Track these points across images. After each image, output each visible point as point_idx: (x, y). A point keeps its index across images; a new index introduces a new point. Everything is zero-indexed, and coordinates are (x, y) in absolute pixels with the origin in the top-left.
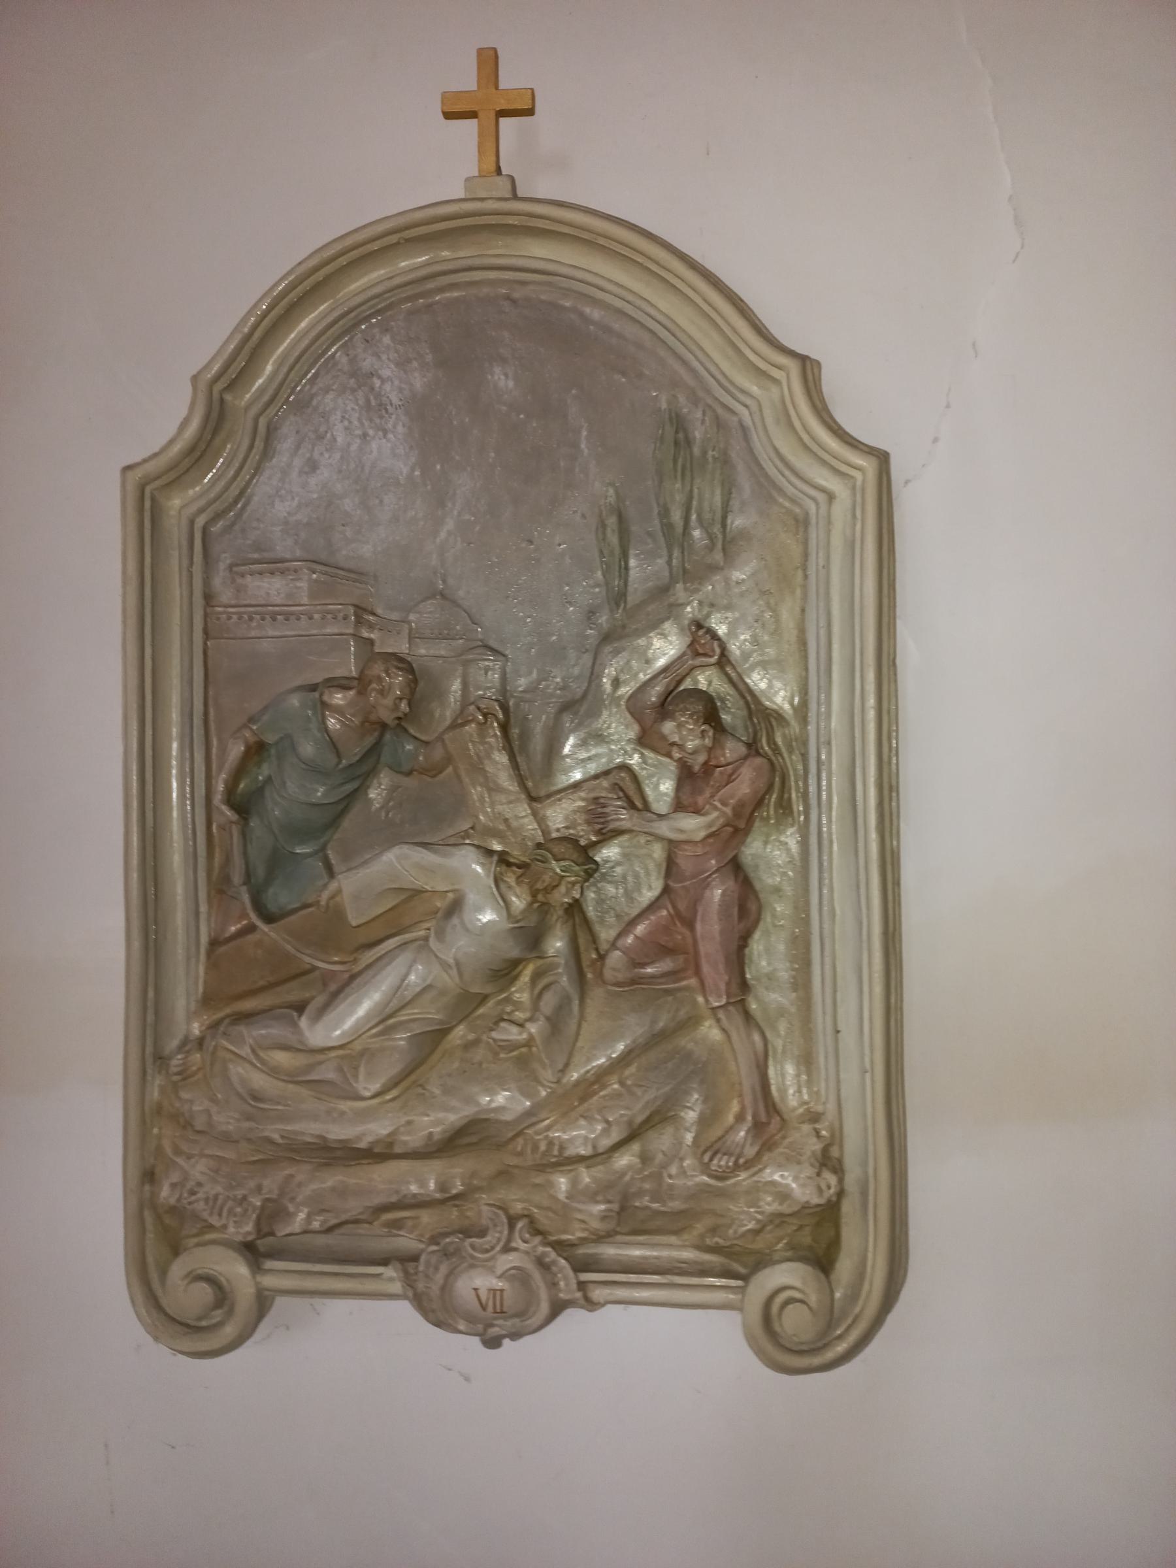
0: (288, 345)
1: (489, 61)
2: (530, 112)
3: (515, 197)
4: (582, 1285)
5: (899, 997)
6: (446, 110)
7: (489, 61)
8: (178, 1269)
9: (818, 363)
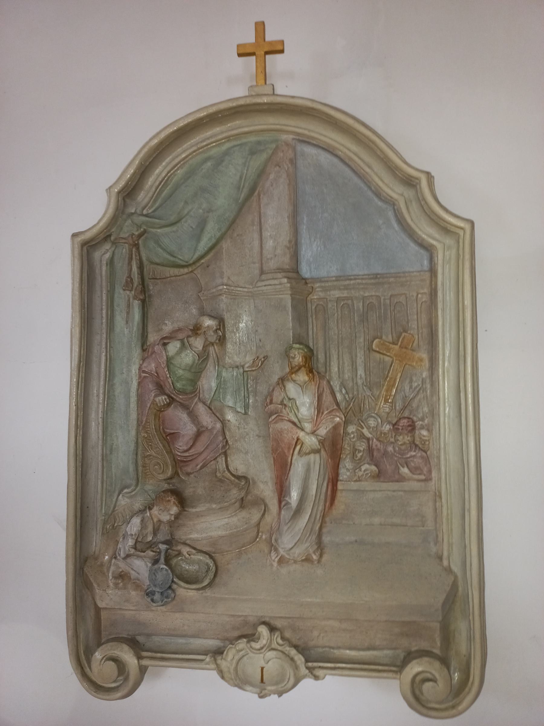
1: (260, 27)
2: (282, 51)
3: (274, 94)
5: (480, 541)
6: (238, 52)
7: (260, 27)
8: (98, 655)
9: (433, 177)
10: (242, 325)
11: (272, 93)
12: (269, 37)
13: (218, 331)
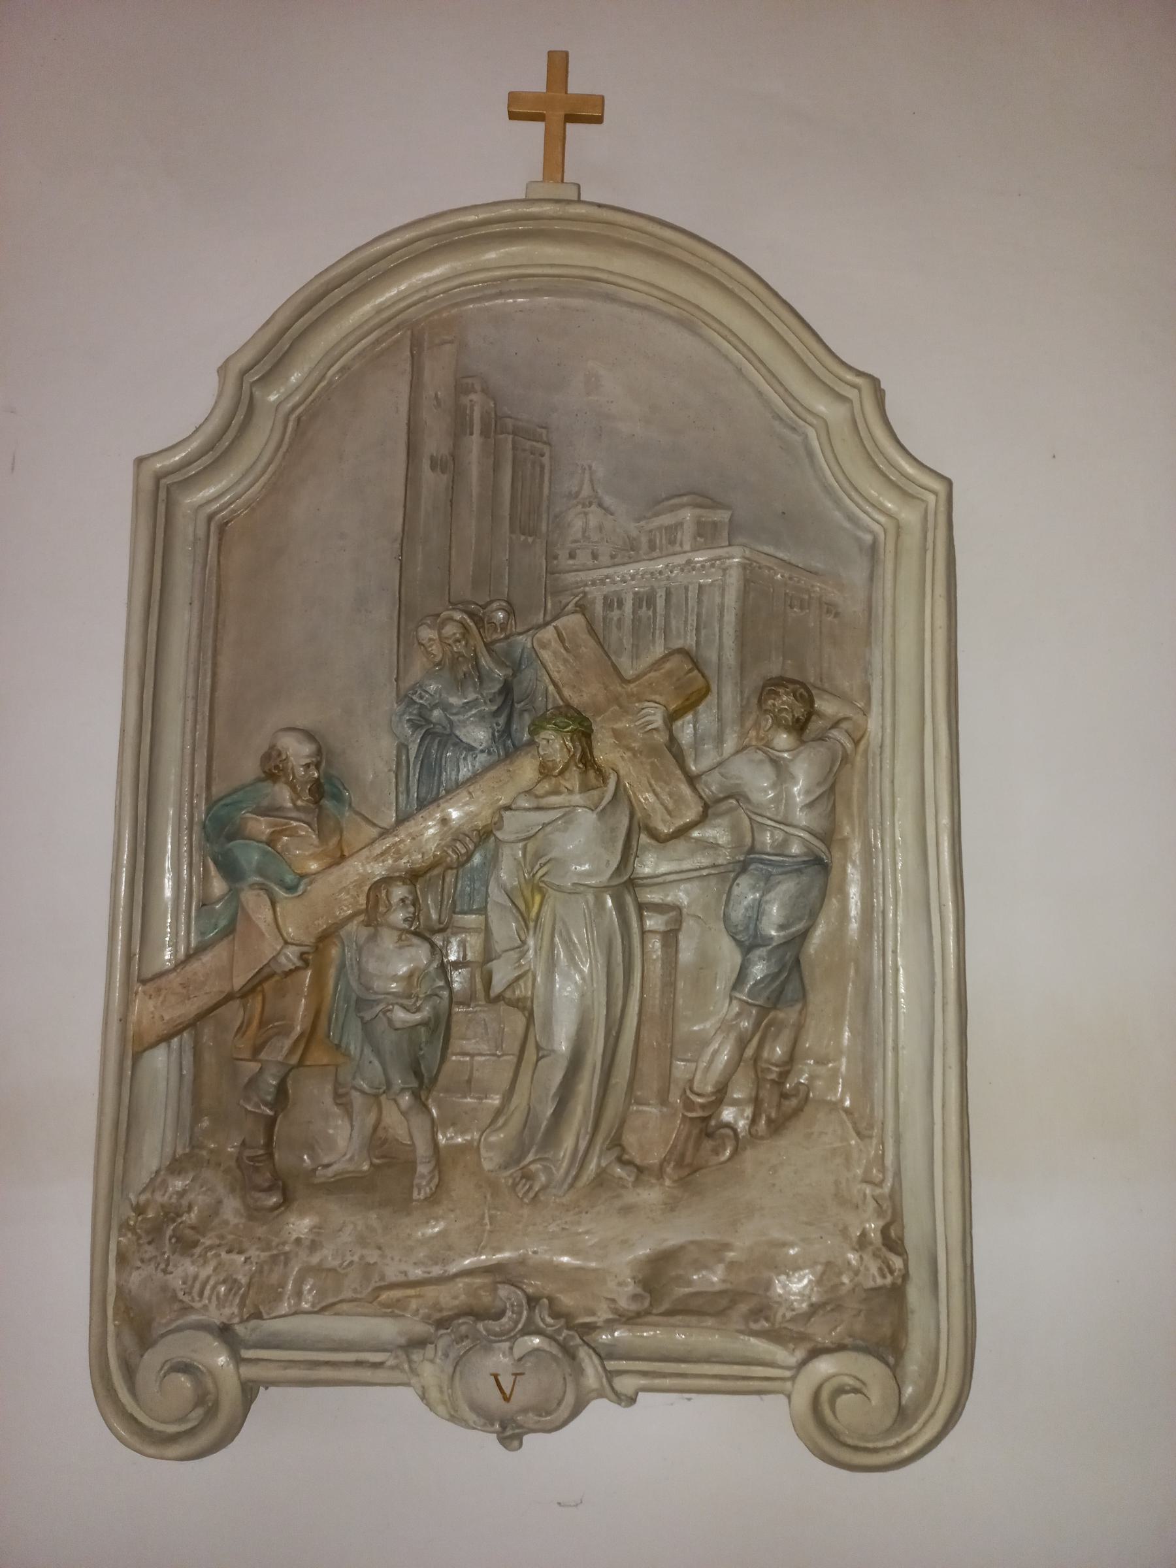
0: (123, 858)
1: (558, 64)
2: (599, 120)
4: (610, 1375)
7: (558, 64)
8: (153, 1360)
10: (309, 1287)
11: (575, 198)
12: (576, 86)
13: (619, 1148)
